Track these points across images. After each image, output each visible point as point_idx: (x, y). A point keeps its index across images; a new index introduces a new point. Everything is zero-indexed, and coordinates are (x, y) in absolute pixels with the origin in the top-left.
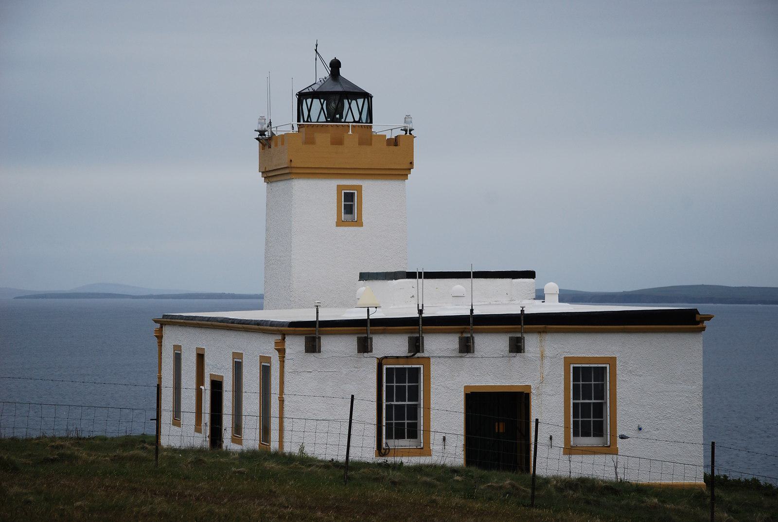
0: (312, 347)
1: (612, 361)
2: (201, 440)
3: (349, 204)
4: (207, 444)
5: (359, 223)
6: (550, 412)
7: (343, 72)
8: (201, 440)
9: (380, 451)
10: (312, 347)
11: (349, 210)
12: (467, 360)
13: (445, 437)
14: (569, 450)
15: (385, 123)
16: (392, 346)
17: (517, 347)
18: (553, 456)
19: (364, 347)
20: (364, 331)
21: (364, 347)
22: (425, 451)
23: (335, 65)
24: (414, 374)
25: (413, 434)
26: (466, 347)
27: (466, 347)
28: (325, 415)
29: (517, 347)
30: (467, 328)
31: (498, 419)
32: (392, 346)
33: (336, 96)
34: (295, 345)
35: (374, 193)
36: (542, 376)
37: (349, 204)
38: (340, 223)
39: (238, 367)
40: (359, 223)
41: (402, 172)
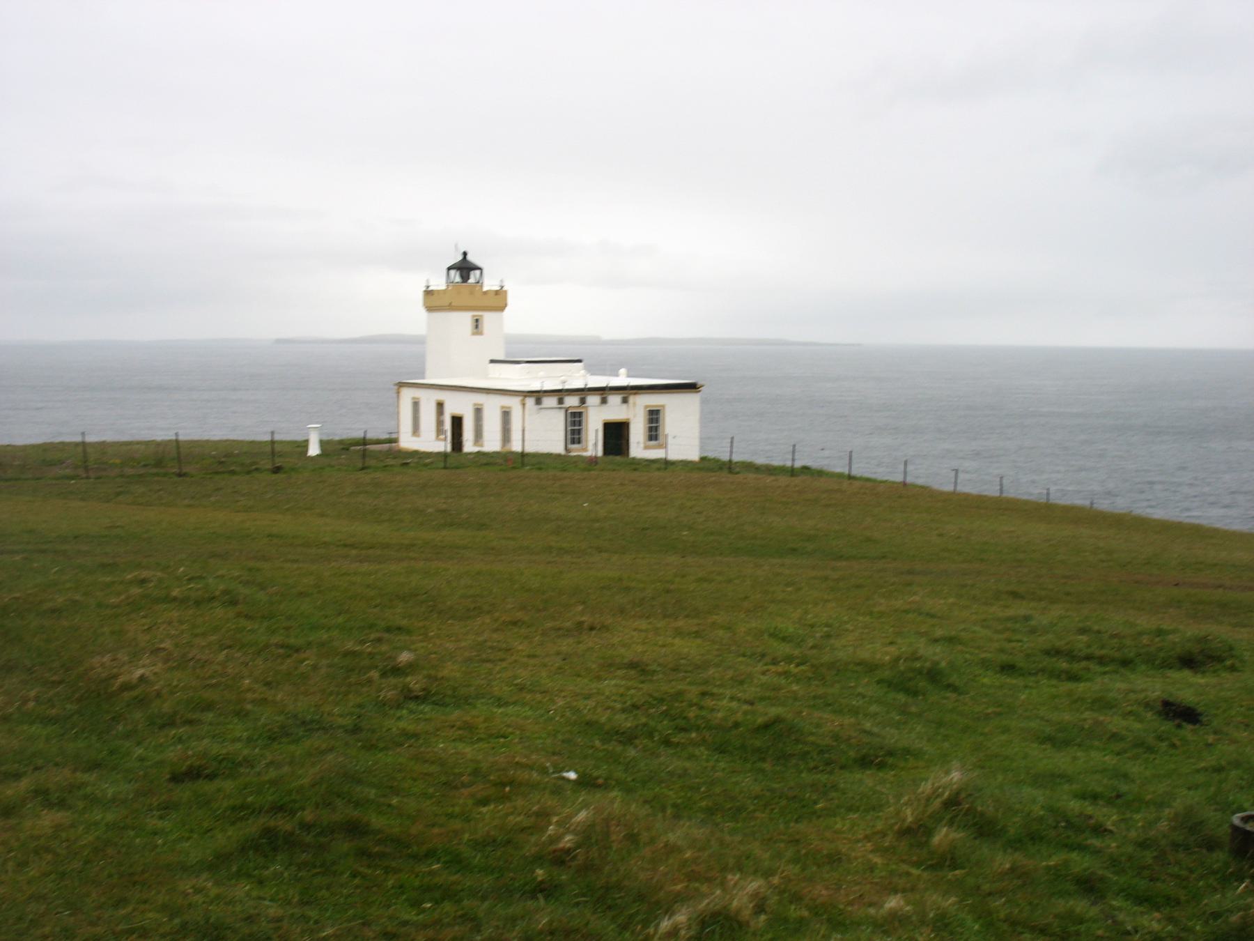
0: (538, 402)
1: (663, 406)
2: (444, 446)
3: (477, 323)
4: (449, 449)
5: (481, 333)
6: (637, 434)
7: (469, 258)
8: (444, 446)
9: (566, 448)
10: (538, 402)
11: (477, 327)
12: (604, 407)
13: (593, 443)
14: (646, 448)
15: (490, 284)
16: (572, 401)
17: (625, 401)
18: (638, 448)
19: (561, 401)
20: (560, 394)
21: (561, 401)
22: (585, 450)
23: (465, 254)
24: (580, 414)
25: (579, 442)
26: (604, 401)
27: (604, 401)
28: (543, 434)
29: (625, 401)
30: (603, 391)
31: (616, 434)
32: (572, 401)
33: (465, 268)
34: (530, 402)
35: (488, 318)
36: (635, 414)
37: (477, 323)
38: (474, 334)
39: (478, 411)
40: (481, 333)
41: (502, 308)
